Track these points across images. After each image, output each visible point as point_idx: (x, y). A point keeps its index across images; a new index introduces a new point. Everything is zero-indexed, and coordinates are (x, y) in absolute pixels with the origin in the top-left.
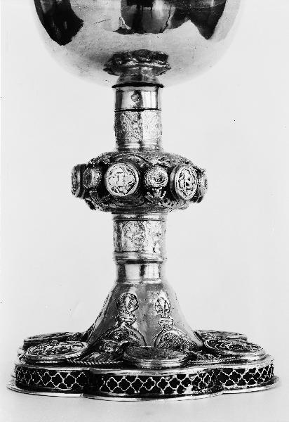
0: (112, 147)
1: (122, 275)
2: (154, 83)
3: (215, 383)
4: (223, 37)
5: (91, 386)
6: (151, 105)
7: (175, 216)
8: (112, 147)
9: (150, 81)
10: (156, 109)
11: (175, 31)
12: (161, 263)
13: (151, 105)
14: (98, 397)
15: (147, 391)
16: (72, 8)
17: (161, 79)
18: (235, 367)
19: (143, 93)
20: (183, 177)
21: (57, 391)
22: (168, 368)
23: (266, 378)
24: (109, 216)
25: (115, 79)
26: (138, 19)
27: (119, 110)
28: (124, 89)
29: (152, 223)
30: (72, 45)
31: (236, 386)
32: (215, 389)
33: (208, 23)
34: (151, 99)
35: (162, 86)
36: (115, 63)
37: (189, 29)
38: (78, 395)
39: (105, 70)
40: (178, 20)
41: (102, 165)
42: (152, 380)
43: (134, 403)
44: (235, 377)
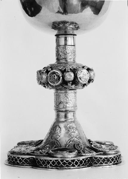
0: (54, 61)
1: (58, 116)
2: (73, 34)
3: (91, 163)
4: (105, 12)
5: (35, 163)
6: (71, 44)
7: (80, 91)
8: (54, 61)
9: (71, 33)
10: (74, 46)
11: (80, 13)
12: (74, 111)
13: (71, 44)
14: (38, 168)
15: (60, 165)
16: (37, 3)
17: (75, 32)
18: (103, 157)
19: (67, 38)
20: (83, 75)
21: (65, 169)
22: (109, 154)
23: (117, 160)
24: (53, 91)
25: (56, 32)
26: (65, 8)
27: (58, 45)
28: (60, 36)
29: (71, 94)
30: (40, 3)
31: (104, 164)
32: (90, 165)
33: (97, 9)
34: (71, 41)
35: (76, 35)
36: (55, 26)
37: (88, 11)
38: (30, 167)
39: (52, 28)
40: (84, 5)
41: (52, 67)
42: (55, 162)
43: (54, 171)
44: (104, 160)
